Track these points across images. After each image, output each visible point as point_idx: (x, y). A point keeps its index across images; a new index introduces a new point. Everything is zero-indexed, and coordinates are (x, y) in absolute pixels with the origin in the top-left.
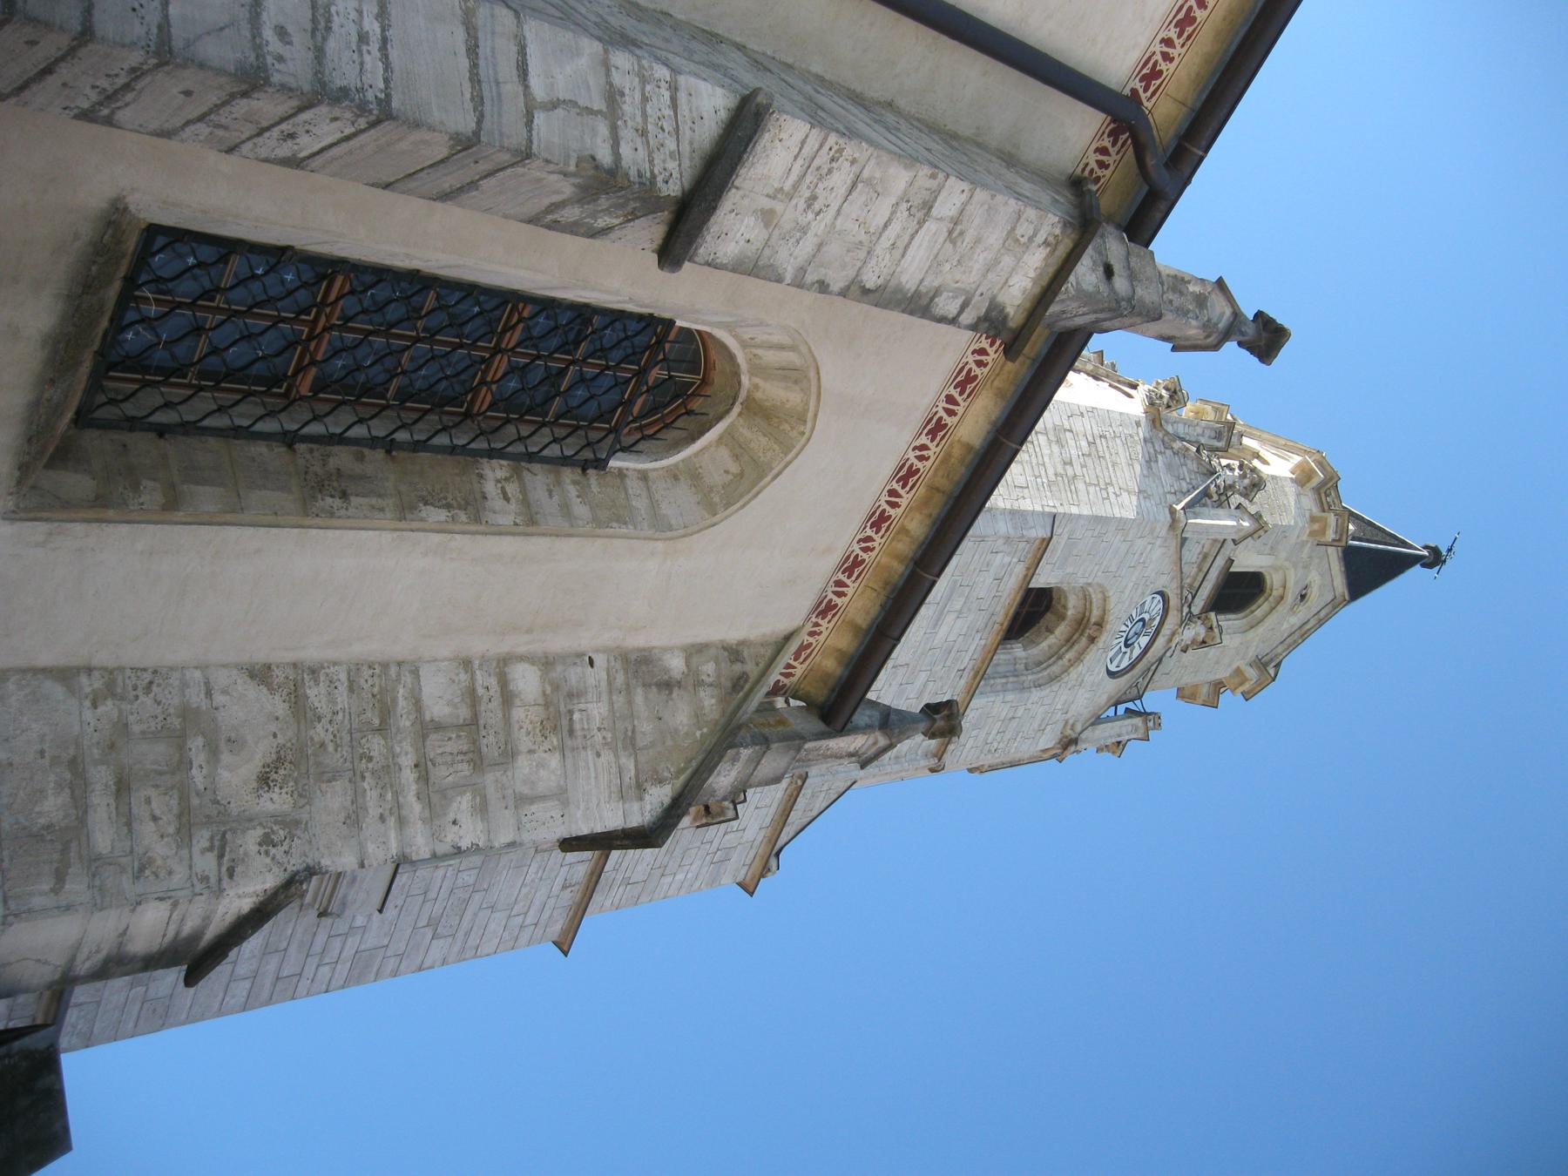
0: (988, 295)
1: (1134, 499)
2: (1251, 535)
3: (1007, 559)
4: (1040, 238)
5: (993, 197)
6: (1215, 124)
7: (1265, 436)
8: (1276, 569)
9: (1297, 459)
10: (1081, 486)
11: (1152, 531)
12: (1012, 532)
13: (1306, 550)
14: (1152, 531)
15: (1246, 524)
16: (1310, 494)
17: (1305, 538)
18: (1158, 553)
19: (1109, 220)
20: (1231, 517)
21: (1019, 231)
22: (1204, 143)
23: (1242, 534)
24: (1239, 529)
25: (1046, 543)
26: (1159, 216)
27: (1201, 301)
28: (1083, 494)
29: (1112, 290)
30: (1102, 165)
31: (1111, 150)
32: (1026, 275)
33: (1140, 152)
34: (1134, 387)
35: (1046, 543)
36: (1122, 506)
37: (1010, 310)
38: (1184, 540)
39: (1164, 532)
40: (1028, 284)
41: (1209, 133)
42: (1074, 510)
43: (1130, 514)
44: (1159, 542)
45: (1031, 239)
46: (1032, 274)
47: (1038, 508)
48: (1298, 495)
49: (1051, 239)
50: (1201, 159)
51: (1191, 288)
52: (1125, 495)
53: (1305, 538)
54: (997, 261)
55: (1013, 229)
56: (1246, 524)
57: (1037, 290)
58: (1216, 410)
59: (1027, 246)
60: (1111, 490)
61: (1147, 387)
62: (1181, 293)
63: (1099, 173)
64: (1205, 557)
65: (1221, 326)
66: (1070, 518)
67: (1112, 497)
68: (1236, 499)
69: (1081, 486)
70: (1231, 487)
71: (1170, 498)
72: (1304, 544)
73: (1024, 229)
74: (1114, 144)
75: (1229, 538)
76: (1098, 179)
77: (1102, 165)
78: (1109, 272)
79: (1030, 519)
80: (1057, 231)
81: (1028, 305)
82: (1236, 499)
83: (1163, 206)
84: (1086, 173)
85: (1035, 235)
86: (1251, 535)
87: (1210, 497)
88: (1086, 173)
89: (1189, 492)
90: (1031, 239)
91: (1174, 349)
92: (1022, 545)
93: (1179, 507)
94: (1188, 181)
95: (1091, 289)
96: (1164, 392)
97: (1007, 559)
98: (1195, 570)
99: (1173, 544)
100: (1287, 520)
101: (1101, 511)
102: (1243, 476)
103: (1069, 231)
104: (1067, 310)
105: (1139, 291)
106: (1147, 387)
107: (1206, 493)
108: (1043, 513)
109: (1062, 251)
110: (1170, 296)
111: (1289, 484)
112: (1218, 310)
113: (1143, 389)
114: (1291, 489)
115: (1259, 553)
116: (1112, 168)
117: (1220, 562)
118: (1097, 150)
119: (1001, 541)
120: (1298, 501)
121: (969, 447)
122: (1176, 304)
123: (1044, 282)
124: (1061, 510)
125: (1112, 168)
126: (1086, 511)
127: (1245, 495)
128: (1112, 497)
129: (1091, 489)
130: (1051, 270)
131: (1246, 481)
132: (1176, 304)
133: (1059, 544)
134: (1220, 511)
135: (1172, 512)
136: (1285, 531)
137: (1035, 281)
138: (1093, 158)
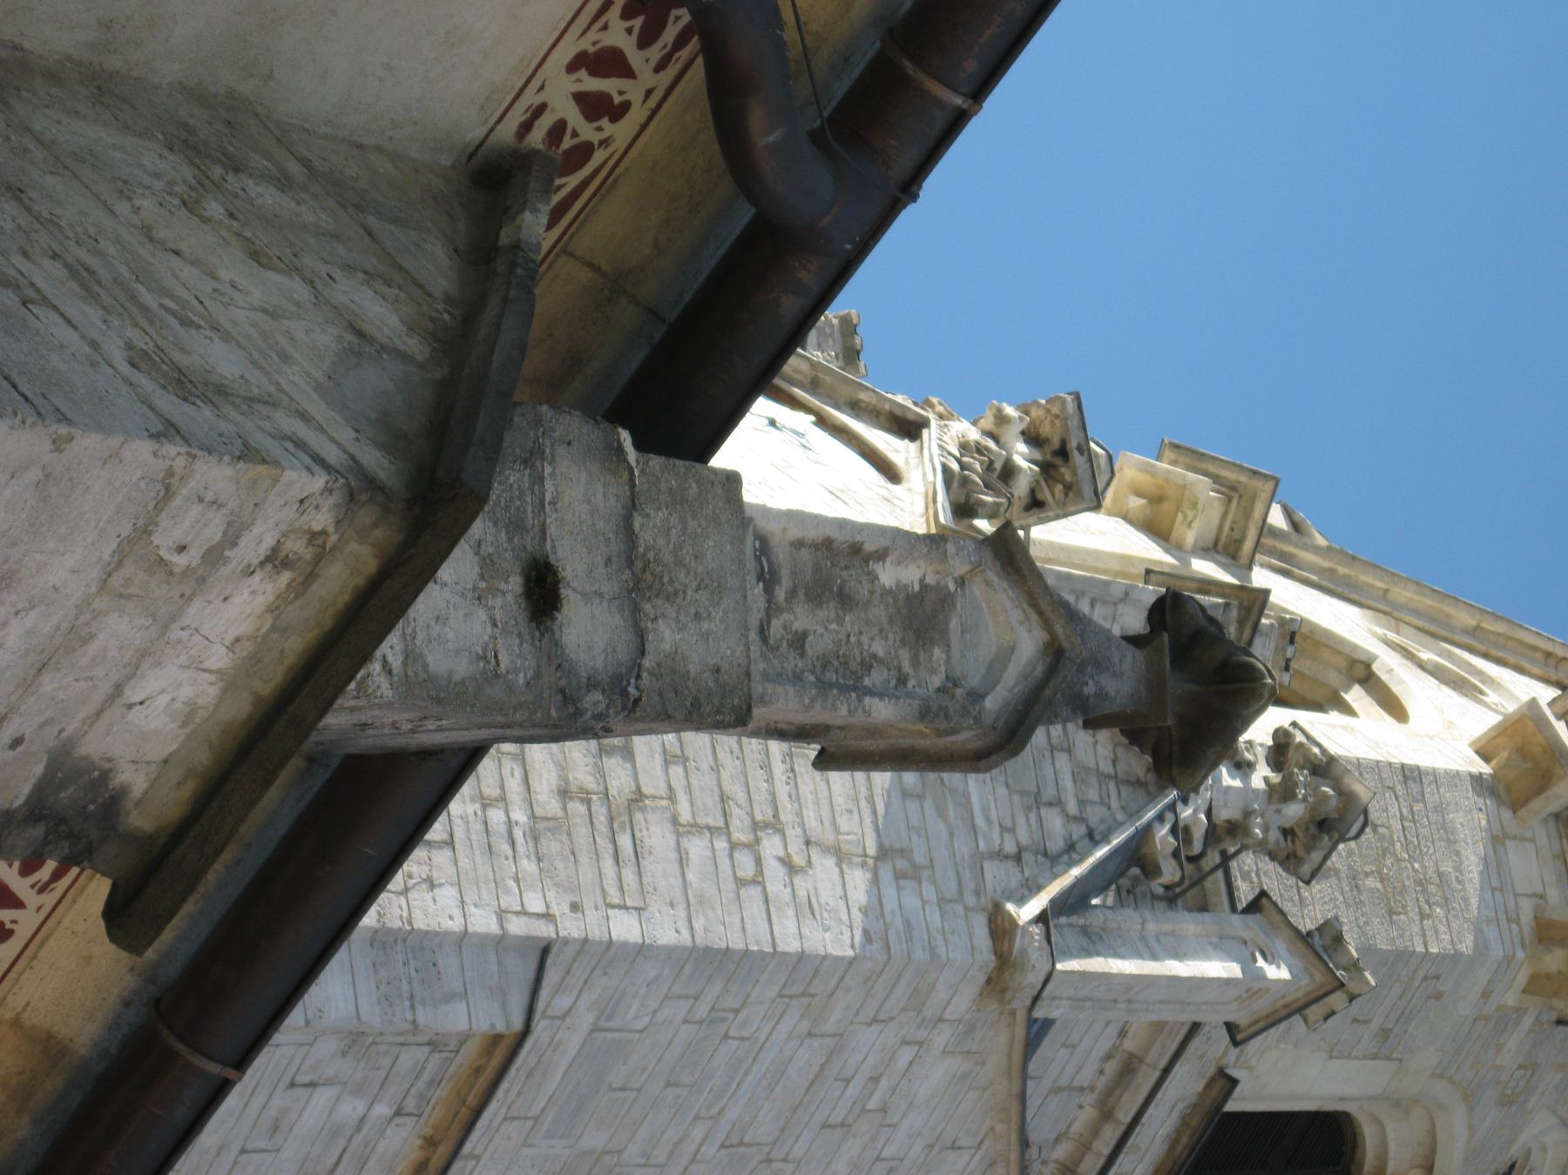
0: (49, 738)
1: (858, 879)
2: (1300, 1009)
3: (351, 1108)
4: (258, 541)
5: (58, 444)
6: (993, 32)
7: (1403, 594)
8: (1400, 1105)
9: (1523, 690)
10: (657, 836)
11: (918, 997)
12: (372, 1015)
13: (1515, 1043)
14: (918, 997)
15: (1277, 972)
16: (1544, 836)
17: (1511, 999)
18: (937, 1073)
19: (553, 389)
20: (1221, 945)
21: (164, 539)
22: (972, 66)
23: (1261, 1006)
24: (1253, 985)
25: (503, 1052)
26: (790, 306)
27: (923, 617)
28: (660, 868)
29: (553, 655)
30: (595, 107)
31: (635, 57)
32: (196, 665)
33: (727, 95)
34: (909, 428)
35: (503, 1052)
36: (808, 909)
37: (133, 779)
38: (1037, 1032)
39: (962, 1004)
40: (205, 691)
41: (993, 32)
42: (625, 928)
43: (835, 939)
44: (942, 1037)
45: (214, 556)
46: (219, 658)
47: (484, 922)
48: (1497, 840)
49: (297, 547)
50: (957, 122)
51: (888, 575)
52: (825, 866)
53: (1511, 999)
54: (77, 636)
55: (144, 531)
56: (1277, 972)
57: (240, 709)
58: (1230, 491)
59: (198, 579)
60: (771, 847)
61: (964, 429)
62: (845, 600)
63: (588, 132)
64: (1129, 1068)
65: (992, 703)
66: (609, 954)
67: (775, 873)
68: (1254, 872)
69: (657, 836)
70: (1236, 829)
71: (995, 872)
72: (1504, 1021)
73: (186, 529)
74: (645, 41)
75: (1214, 1019)
76: (583, 152)
77: (595, 107)
78: (542, 591)
79: (449, 964)
80: (322, 519)
81: (203, 758)
82: (1254, 872)
83: (809, 274)
84: (536, 138)
85: (231, 539)
86: (1300, 1009)
87: (1150, 869)
88: (536, 138)
89: (1055, 860)
90: (214, 556)
91: (824, 761)
92: (408, 1059)
93: (1026, 912)
94: (908, 190)
95: (462, 668)
96: (1021, 455)
97: (351, 1108)
98: (1089, 1113)
99: (1000, 1041)
100: (1445, 935)
101: (733, 927)
102: (1282, 793)
103: (366, 515)
104: (374, 708)
105: (666, 636)
106: (964, 429)
107: (1136, 857)
108: (500, 943)
109: (337, 583)
110: (802, 618)
111: (1468, 797)
112: (989, 642)
113: (950, 434)
114: (1471, 821)
115: (1334, 1053)
116: (636, 116)
117: (1185, 1085)
118: (579, 63)
119: (328, 1047)
120: (1494, 865)
121: (50, 1048)
122: (818, 644)
123: (269, 682)
124: (571, 928)
125: (636, 116)
126: (667, 931)
127: (1289, 861)
128: (775, 873)
129: (697, 848)
130: (295, 645)
131: (1294, 811)
132: (818, 644)
133: (559, 1044)
134: (1188, 923)
135: (1001, 929)
136: (1429, 977)
137: (231, 682)
138: (561, 94)
